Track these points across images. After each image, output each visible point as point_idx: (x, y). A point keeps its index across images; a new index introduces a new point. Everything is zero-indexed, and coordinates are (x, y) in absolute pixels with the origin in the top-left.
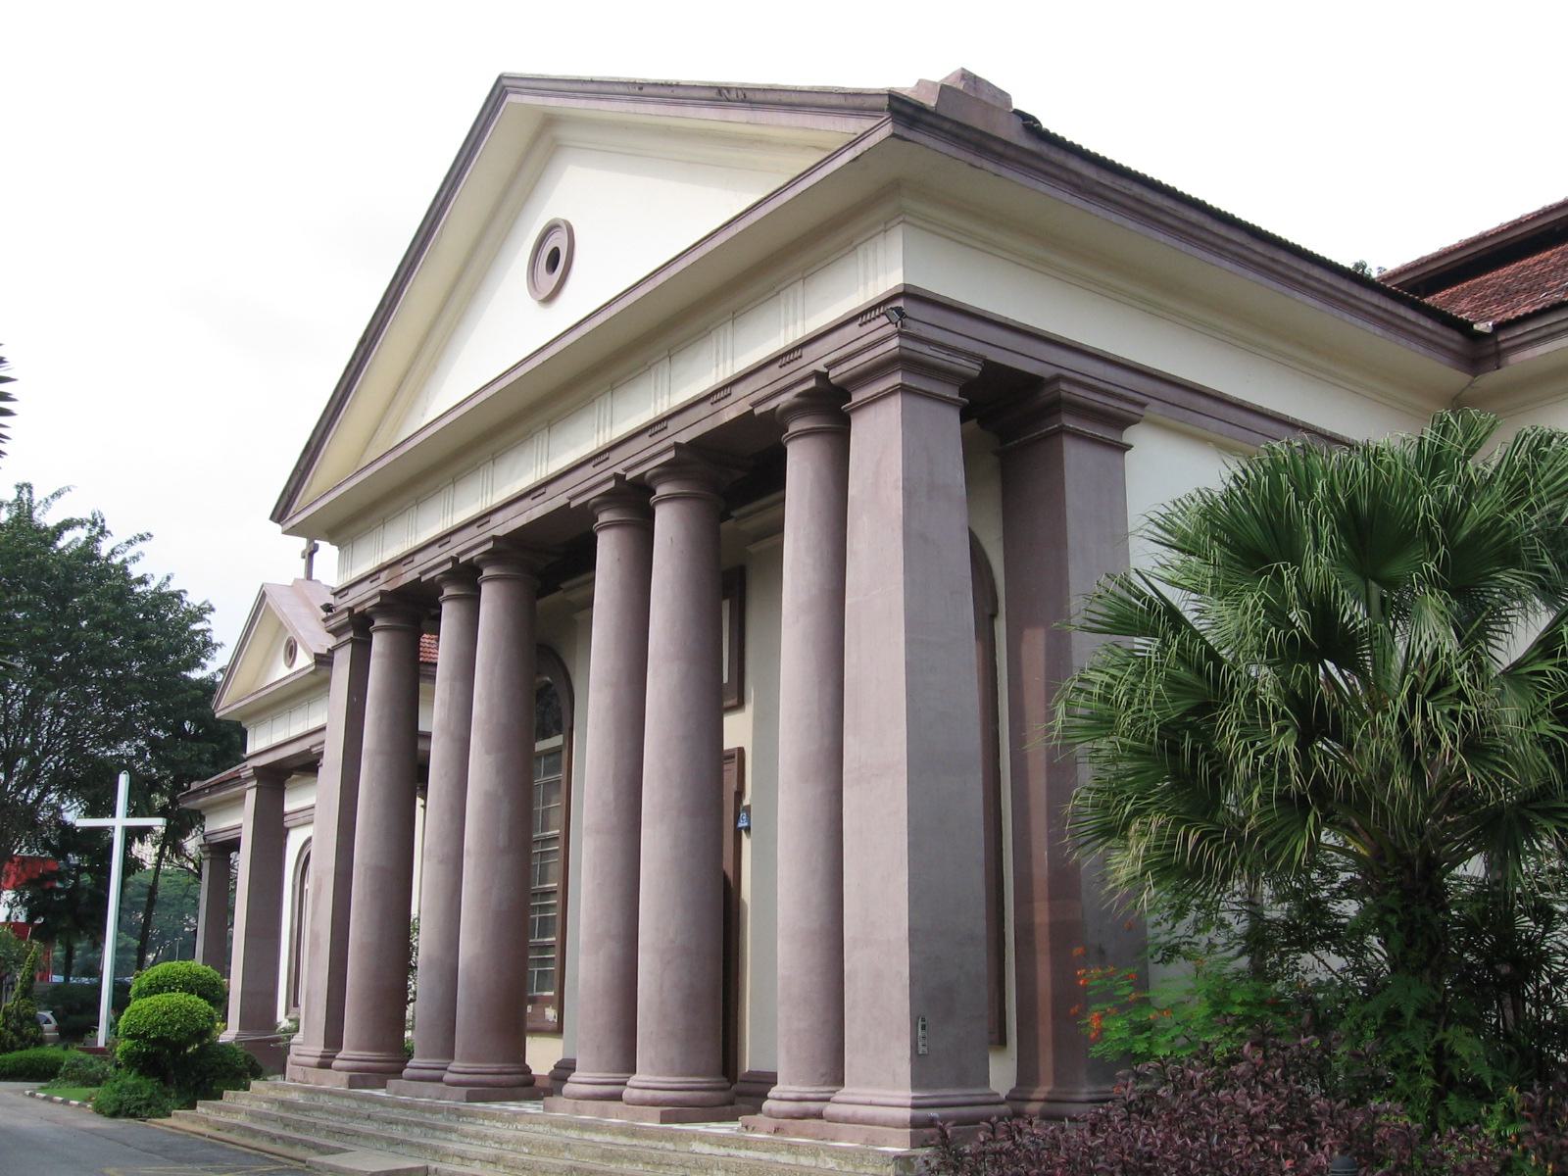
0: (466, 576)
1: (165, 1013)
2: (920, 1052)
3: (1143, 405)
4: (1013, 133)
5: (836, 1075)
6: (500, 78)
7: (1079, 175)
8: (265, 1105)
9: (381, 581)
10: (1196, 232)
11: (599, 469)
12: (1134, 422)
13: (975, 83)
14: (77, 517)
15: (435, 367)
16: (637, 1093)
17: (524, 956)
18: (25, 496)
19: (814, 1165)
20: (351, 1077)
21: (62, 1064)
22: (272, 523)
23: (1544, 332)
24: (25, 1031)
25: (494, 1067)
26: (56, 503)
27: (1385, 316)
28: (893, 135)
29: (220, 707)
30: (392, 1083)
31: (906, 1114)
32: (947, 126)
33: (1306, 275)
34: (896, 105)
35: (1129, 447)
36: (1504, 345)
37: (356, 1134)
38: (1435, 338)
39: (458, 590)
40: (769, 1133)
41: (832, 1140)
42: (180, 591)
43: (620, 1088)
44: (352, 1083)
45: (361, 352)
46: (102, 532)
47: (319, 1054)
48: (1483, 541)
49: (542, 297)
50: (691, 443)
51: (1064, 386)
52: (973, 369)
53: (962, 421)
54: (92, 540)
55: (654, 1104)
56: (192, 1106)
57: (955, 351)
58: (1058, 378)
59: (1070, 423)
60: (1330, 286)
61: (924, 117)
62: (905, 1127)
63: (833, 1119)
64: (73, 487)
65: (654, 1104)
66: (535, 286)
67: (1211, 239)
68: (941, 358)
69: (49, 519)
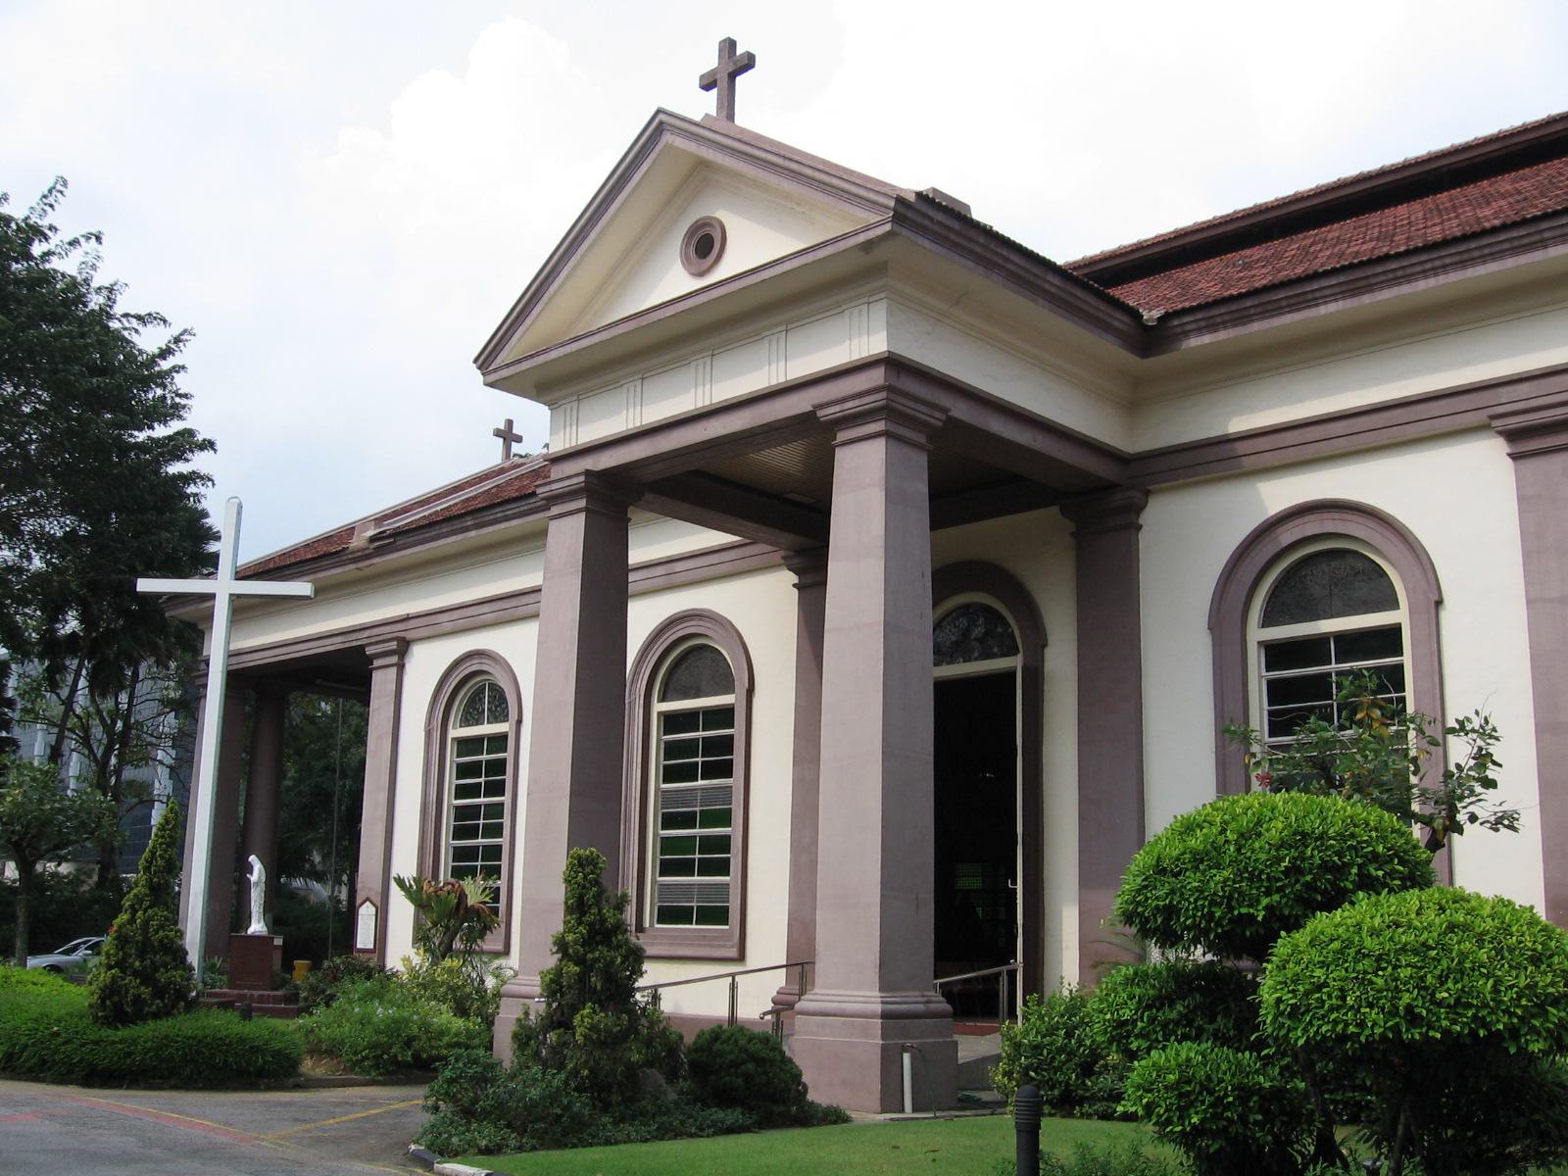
22: (227, 596)
34: (902, 210)
48: (162, 784)
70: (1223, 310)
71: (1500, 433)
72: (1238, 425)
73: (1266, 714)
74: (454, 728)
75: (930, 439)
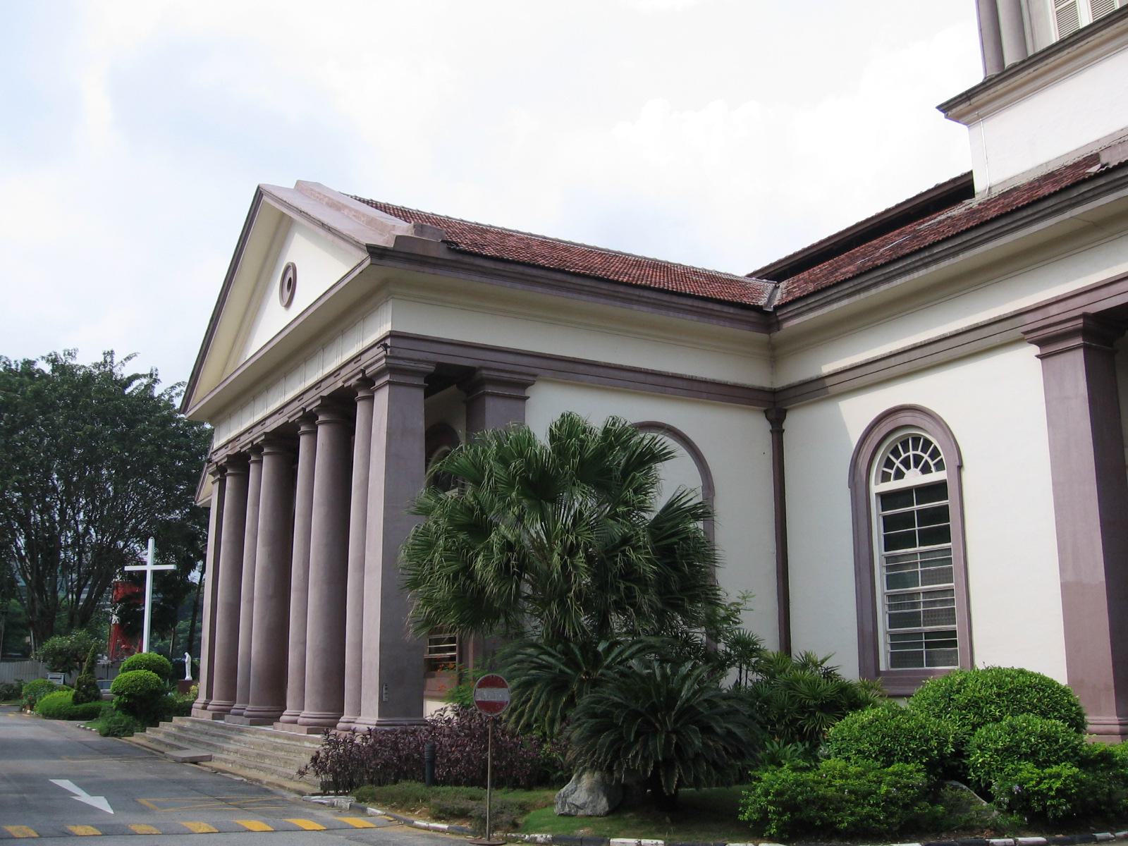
1: (133, 681)
8: (173, 729)
9: (229, 448)
12: (532, 384)
13: (422, 228)
14: (140, 373)
15: (249, 333)
18: (109, 359)
20: (213, 714)
21: (100, 710)
23: (796, 312)
24: (89, 692)
25: (265, 708)
26: (128, 363)
28: (371, 264)
29: (200, 499)
30: (227, 717)
32: (401, 255)
33: (639, 296)
35: (529, 397)
36: (780, 318)
37: (197, 741)
39: (257, 457)
43: (296, 718)
44: (214, 717)
45: (212, 326)
46: (156, 381)
47: (203, 702)
50: (330, 396)
51: (484, 372)
52: (431, 368)
53: (426, 397)
54: (149, 387)
56: (144, 731)
58: (481, 368)
59: (489, 389)
61: (387, 253)
64: (139, 353)
68: (410, 365)
69: (125, 372)
70: (927, 254)
71: (1031, 343)
72: (827, 369)
73: (882, 538)
74: (876, 484)
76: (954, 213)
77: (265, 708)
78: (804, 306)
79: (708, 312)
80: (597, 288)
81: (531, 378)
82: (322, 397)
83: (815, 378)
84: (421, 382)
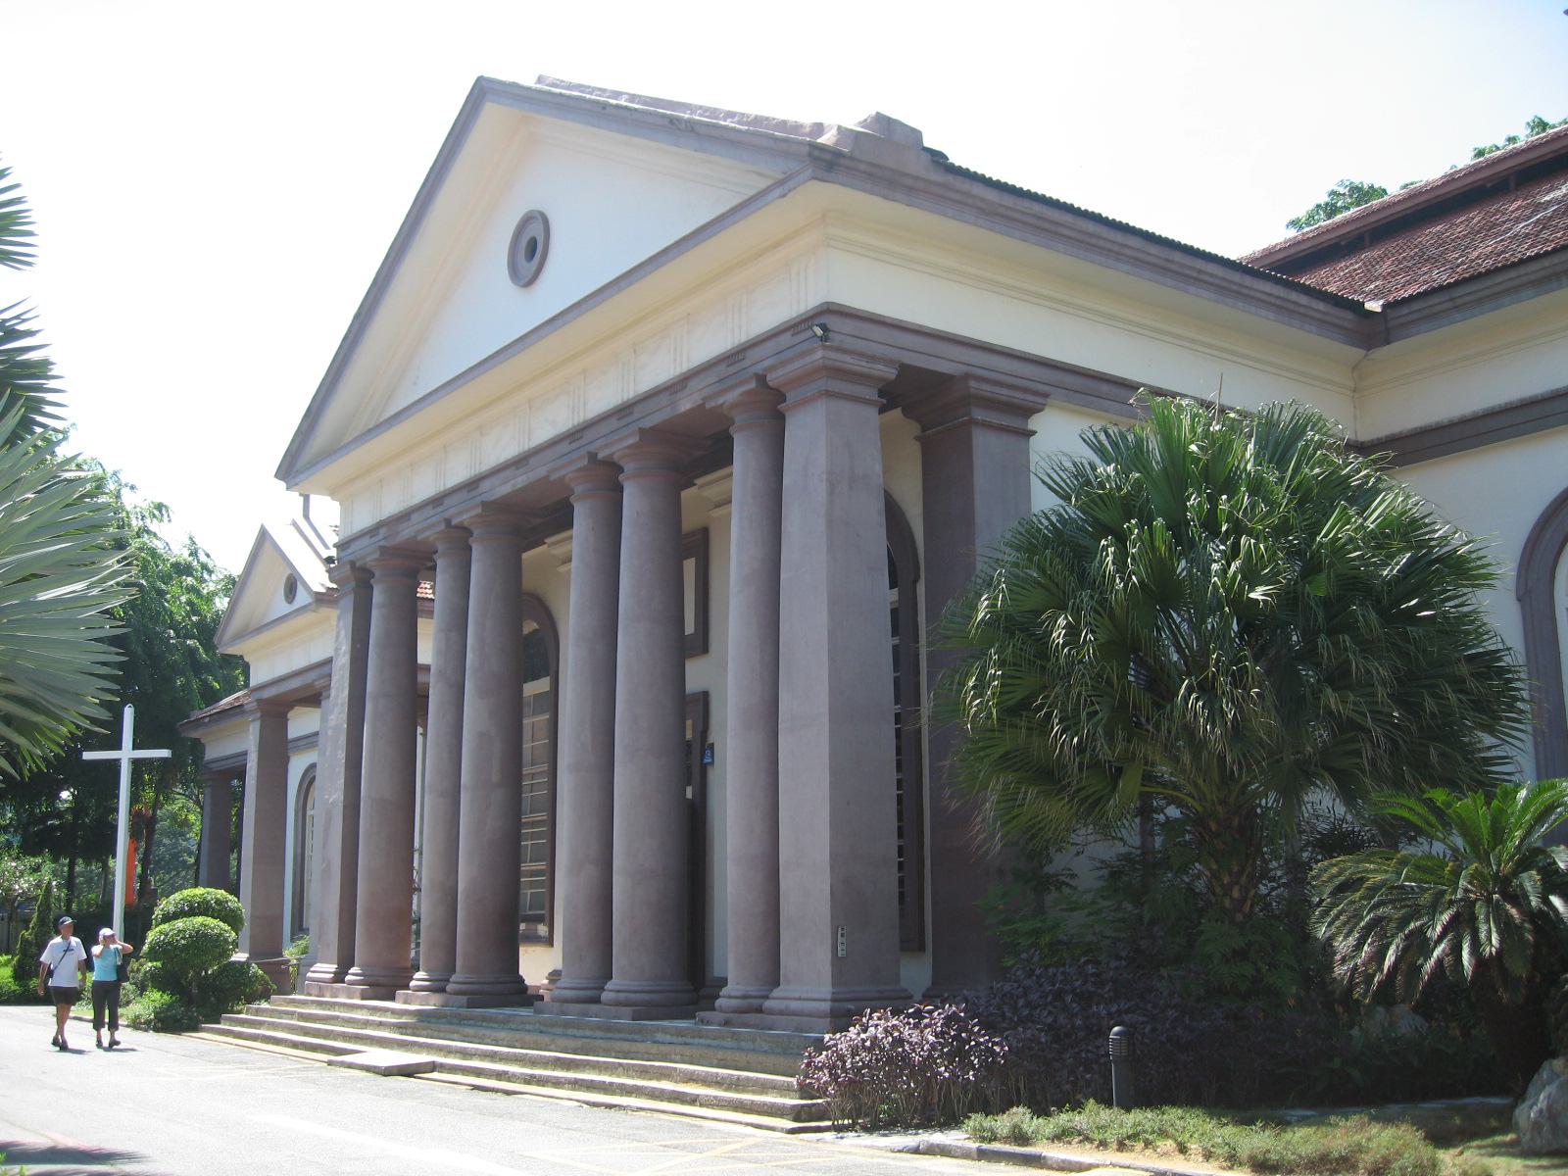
0: (460, 538)
2: (840, 955)
3: (1046, 395)
4: (920, 168)
5: (774, 980)
6: (480, 79)
7: (983, 200)
10: (1094, 241)
11: (575, 445)
16: (612, 995)
17: (518, 882)
19: (752, 1047)
25: (636, 983)
27: (1278, 302)
31: (826, 1006)
32: (862, 167)
33: (1200, 271)
34: (816, 153)
35: (1033, 433)
38: (1328, 318)
40: (720, 1025)
41: (771, 1029)
42: (165, 506)
49: (522, 282)
51: (973, 384)
52: (891, 373)
55: (627, 1004)
57: (873, 359)
58: (967, 377)
59: (978, 414)
60: (1224, 279)
62: (825, 1017)
63: (771, 1012)
65: (627, 1004)
66: (515, 273)
67: (1108, 246)
75: (881, 394)
76: (524, 477)
77: (636, 983)
78: (1444, 302)
79: (1291, 306)
80: (1144, 252)
81: (1039, 400)
82: (642, 431)
83: (1446, 421)
84: (872, 393)
